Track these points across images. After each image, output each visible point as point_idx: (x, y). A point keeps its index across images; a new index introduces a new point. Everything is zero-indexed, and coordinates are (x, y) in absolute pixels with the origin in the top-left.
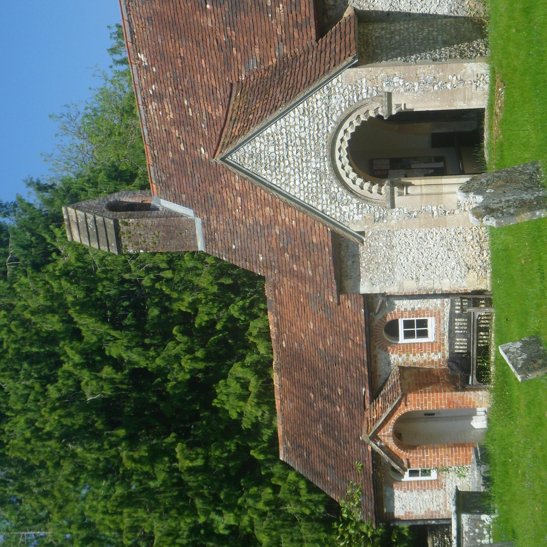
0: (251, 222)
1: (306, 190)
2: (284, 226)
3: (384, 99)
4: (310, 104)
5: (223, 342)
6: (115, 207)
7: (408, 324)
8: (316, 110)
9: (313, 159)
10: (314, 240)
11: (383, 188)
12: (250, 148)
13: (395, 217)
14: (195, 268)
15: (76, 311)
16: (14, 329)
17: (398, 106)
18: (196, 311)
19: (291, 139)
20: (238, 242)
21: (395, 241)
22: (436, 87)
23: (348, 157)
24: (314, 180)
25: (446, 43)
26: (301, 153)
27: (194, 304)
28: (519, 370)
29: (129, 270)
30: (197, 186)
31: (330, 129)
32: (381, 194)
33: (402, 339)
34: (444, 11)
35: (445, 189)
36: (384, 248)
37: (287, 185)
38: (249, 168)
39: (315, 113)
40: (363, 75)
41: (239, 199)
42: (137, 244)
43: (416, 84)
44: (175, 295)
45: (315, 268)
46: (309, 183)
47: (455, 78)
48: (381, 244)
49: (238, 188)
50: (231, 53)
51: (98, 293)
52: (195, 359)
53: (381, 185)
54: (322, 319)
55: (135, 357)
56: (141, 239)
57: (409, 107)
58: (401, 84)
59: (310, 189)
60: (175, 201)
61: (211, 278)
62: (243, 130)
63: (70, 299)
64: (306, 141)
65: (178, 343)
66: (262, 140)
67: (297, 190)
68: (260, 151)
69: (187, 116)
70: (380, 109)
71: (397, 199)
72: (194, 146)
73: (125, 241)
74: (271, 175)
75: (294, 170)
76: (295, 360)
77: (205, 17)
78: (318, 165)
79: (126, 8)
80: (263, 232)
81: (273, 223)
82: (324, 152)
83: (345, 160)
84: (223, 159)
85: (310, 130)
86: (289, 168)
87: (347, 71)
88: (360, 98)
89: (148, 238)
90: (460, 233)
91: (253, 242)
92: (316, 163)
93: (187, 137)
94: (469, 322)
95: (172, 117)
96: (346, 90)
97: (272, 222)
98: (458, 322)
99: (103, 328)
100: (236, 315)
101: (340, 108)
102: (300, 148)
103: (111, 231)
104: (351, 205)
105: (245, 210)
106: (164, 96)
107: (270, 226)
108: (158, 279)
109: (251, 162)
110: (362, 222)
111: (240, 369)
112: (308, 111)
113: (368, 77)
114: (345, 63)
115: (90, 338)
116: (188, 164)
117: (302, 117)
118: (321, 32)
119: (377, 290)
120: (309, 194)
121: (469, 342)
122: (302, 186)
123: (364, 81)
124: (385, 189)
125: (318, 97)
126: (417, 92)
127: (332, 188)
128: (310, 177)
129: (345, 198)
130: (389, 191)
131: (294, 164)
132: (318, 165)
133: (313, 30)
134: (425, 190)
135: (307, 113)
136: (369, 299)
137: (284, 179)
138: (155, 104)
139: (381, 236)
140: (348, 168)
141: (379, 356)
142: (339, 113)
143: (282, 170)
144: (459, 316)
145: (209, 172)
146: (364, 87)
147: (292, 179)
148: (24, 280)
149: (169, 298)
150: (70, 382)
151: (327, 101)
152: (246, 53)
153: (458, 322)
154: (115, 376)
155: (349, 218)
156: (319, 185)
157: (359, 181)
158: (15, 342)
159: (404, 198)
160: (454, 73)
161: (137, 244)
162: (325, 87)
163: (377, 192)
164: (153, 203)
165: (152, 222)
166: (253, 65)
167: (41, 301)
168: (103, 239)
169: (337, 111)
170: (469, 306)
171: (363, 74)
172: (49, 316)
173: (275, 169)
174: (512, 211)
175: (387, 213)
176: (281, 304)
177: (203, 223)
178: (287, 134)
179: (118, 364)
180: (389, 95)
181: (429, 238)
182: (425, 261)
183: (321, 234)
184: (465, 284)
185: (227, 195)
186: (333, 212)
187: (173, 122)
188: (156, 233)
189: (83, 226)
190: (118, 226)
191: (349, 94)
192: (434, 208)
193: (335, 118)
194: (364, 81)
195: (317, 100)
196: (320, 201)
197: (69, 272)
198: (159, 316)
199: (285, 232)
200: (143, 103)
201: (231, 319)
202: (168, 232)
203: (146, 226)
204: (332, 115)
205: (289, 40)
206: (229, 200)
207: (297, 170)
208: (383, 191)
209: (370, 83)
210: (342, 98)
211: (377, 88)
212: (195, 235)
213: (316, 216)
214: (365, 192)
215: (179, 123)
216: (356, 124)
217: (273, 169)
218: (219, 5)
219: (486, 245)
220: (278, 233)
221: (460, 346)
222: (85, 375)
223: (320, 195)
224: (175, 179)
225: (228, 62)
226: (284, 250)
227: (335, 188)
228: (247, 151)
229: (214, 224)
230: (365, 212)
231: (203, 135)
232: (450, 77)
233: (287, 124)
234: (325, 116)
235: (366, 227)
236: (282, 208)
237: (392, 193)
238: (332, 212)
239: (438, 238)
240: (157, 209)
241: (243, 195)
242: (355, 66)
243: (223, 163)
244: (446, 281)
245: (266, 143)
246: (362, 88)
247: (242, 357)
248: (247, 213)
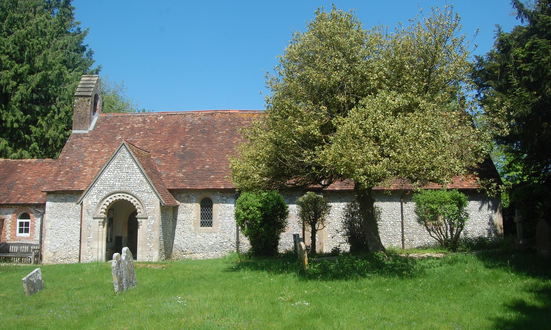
5: (19, 136)
6: (96, 97)
7: (27, 224)
14: (58, 129)
15: (44, 74)
16: (38, 46)
17: (141, 222)
18: (37, 127)
20: (76, 148)
21: (72, 219)
25: (165, 243)
27: (42, 127)
28: (28, 279)
29: (60, 100)
33: (19, 221)
34: (175, 242)
35: (100, 242)
42: (79, 104)
44: (46, 118)
45: (61, 181)
50: (162, 154)
51: (50, 85)
52: (12, 123)
53: (104, 213)
54: (33, 183)
55: (16, 96)
56: (81, 106)
57: (140, 227)
61: (52, 135)
62: (135, 154)
63: (50, 73)
65: (22, 117)
67: (106, 175)
71: (97, 220)
73: (80, 99)
76: (11, 170)
82: (123, 189)
83: (118, 198)
84: (123, 144)
94: (26, 253)
97: (85, 164)
98: (27, 248)
99: (34, 85)
100: (32, 145)
103: (86, 94)
105: (91, 152)
108: (55, 113)
111: (4, 143)
114: (162, 200)
115: (30, 77)
118: (171, 191)
119: (47, 210)
121: (15, 253)
124: (103, 215)
125: (148, 188)
133: (172, 188)
134: (101, 233)
136: (43, 206)
138: (141, 120)
140: (114, 199)
141: (11, 209)
144: (30, 249)
148: (61, 55)
149: (45, 115)
150: (8, 66)
152: (163, 159)
153: (27, 248)
154: (10, 86)
157: (108, 204)
158: (32, 45)
159: (98, 224)
161: (79, 104)
163: (101, 212)
166: (157, 162)
167: (50, 59)
168: (82, 90)
170: (35, 253)
171: (157, 207)
172: (42, 61)
174: (119, 274)
176: (41, 165)
179: (15, 88)
180: (147, 218)
182: (60, 233)
184: (47, 251)
187: (133, 127)
189: (89, 82)
193: (138, 194)
197: (62, 75)
198: (35, 110)
201: (30, 143)
202: (83, 118)
205: (168, 177)
212: (80, 130)
214: (102, 206)
215: (132, 128)
216: (134, 203)
219: (66, 262)
221: (12, 248)
222: (11, 73)
225: (158, 151)
226: (71, 168)
227: (106, 193)
229: (85, 138)
237: (100, 218)
238: (94, 191)
241: (99, 152)
242: (160, 204)
244: (49, 242)
247: (10, 145)
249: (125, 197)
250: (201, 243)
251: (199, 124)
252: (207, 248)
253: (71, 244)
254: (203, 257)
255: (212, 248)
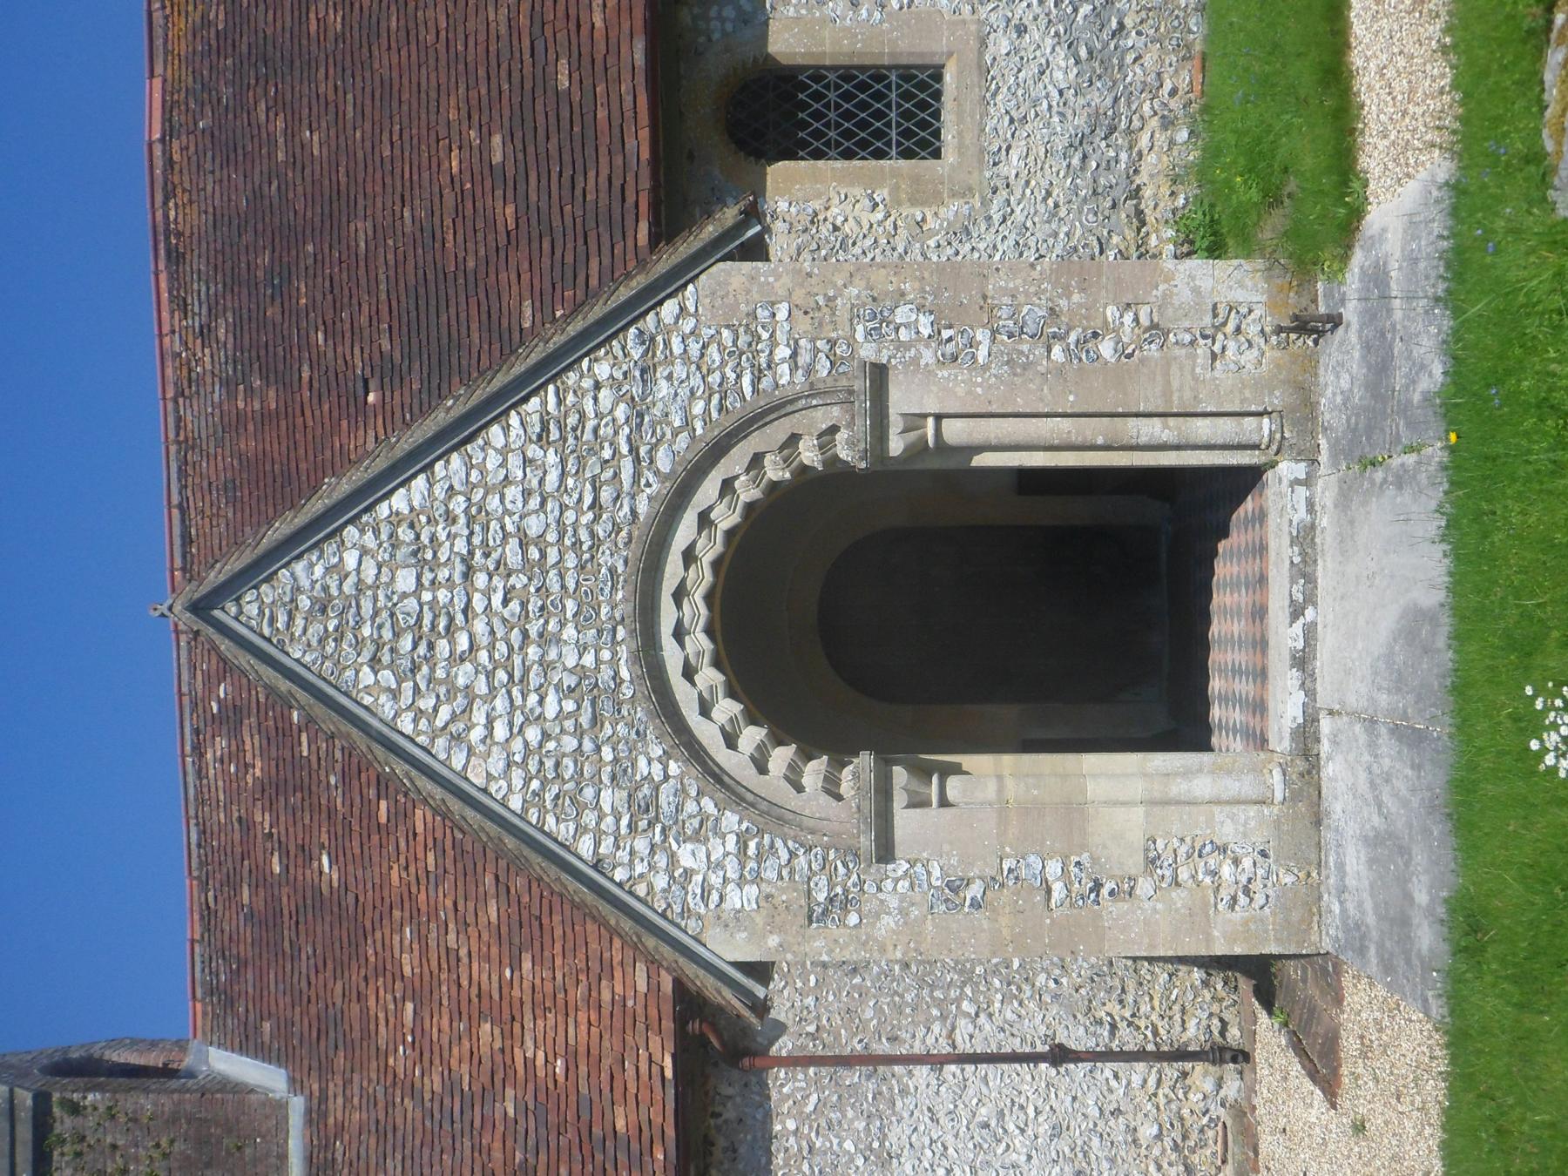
0: (437, 1087)
1: (533, 767)
2: (531, 1086)
3: (858, 385)
4: (570, 398)
8: (590, 425)
9: (570, 632)
10: (620, 1124)
11: (847, 773)
12: (319, 571)
13: (894, 903)
17: (914, 421)
19: (485, 543)
21: (897, 1136)
22: (1057, 352)
23: (709, 598)
24: (569, 724)
26: (524, 605)
30: (304, 984)
31: (643, 507)
32: (839, 798)
36: (860, 1162)
37: (457, 738)
38: (308, 659)
39: (588, 435)
40: (780, 288)
41: (409, 1006)
43: (982, 335)
46: (546, 736)
47: (1128, 318)
48: (849, 1145)
49: (407, 970)
53: (838, 764)
58: (926, 331)
59: (549, 763)
60: (243, 1049)
64: (543, 555)
66: (369, 540)
67: (496, 764)
68: (360, 587)
69: (296, 761)
70: (841, 436)
71: (905, 820)
72: (307, 854)
74: (395, 695)
75: (490, 675)
77: (361, 432)
78: (588, 660)
79: (180, 468)
80: (467, 1117)
81: (499, 1076)
82: (617, 602)
85: (563, 508)
86: (468, 667)
87: (721, 265)
88: (765, 383)
89: (137, 1160)
90: (1117, 1112)
91: (436, 1159)
92: (582, 650)
93: (291, 830)
95: (258, 773)
96: (713, 349)
97: (500, 1073)
101: (688, 422)
102: (518, 581)
104: (715, 842)
105: (423, 1050)
106: (245, 712)
107: (489, 1093)
109: (315, 630)
110: (759, 920)
112: (561, 428)
113: (799, 296)
114: (710, 231)
116: (286, 918)
117: (533, 451)
120: (544, 783)
122: (517, 745)
123: (782, 314)
125: (603, 370)
126: (985, 368)
127: (642, 762)
128: (551, 709)
129: (691, 807)
130: (869, 777)
131: (491, 648)
132: (588, 660)
135: (554, 434)
137: (444, 713)
138: (221, 743)
139: (850, 1114)
140: (699, 642)
142: (682, 441)
143: (440, 673)
145: (336, 932)
146: (781, 337)
147: (479, 717)
151: (636, 391)
155: (705, 898)
156: (588, 745)
160: (1129, 298)
162: (632, 330)
163: (822, 792)
164: (188, 1061)
165: (155, 1104)
169: (675, 434)
173: (415, 669)
175: (861, 883)
177: (309, 1111)
178: (471, 520)
180: (879, 374)
181: (1011, 1127)
183: (644, 1095)
185: (379, 1001)
186: (640, 868)
188: (164, 1142)
190: (49, 1112)
191: (723, 363)
192: (1053, 868)
194: (782, 314)
195: (597, 386)
196: (589, 818)
199: (531, 1106)
200: (193, 748)
203: (135, 1120)
204: (653, 448)
206: (381, 1015)
207: (501, 675)
208: (846, 788)
209: (804, 324)
210: (696, 380)
211: (833, 343)
212: (283, 1157)
213: (565, 877)
214: (773, 783)
216: (747, 492)
217: (406, 663)
218: (397, 380)
220: (511, 1112)
223: (589, 792)
224: (250, 976)
227: (653, 760)
228: (305, 583)
230: (771, 875)
231: (331, 812)
232: (1111, 312)
233: (475, 476)
234: (625, 449)
235: (773, 941)
236: (528, 1017)
237: (884, 792)
238: (636, 868)
239: (1044, 1129)
240: (191, 1075)
241: (420, 993)
243: (198, 625)
245: (383, 556)
246: (773, 343)
248: (426, 1056)
249: (690, 577)
250: (1060, 144)
251: (236, 329)
252: (1098, 97)
253: (1078, 1127)
254: (1167, 123)
255: (1100, 63)
